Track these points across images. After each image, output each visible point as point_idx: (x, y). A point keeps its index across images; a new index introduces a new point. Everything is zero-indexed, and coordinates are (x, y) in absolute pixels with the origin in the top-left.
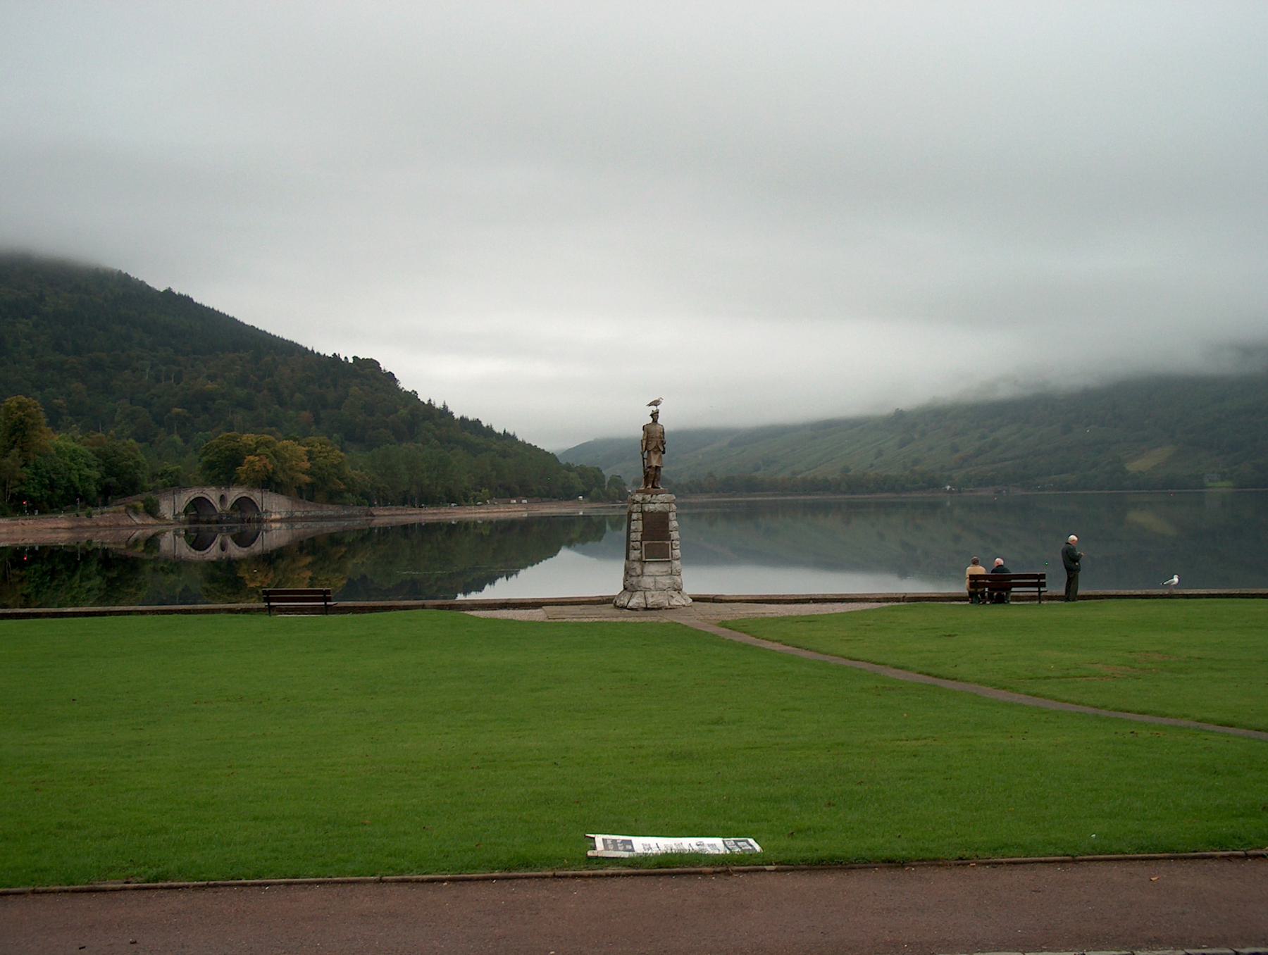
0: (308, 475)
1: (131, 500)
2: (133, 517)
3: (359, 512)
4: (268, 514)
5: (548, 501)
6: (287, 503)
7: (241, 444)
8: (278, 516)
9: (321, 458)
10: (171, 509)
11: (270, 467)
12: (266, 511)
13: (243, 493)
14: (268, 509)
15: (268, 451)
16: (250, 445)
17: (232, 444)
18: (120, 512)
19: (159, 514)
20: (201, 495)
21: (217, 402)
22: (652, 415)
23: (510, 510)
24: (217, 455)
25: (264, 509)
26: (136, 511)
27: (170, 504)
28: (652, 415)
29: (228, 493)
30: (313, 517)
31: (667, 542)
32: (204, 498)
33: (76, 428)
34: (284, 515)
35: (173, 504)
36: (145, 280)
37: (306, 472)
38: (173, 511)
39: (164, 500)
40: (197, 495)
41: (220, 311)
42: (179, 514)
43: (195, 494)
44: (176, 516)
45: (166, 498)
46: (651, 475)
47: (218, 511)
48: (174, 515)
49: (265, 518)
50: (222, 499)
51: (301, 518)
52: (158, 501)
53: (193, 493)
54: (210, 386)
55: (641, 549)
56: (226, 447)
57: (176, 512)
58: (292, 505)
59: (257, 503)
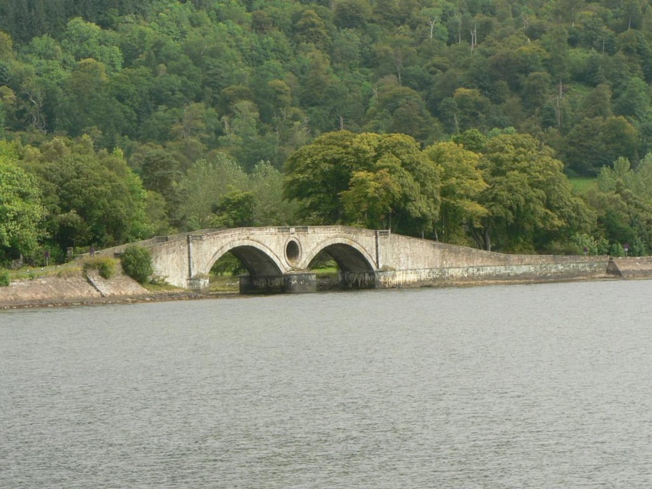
0: (480, 202)
1: (107, 255)
2: (95, 283)
3: (590, 266)
4: (390, 273)
5: (614, 278)
6: (431, 254)
7: (350, 150)
8: (412, 277)
9: (516, 172)
10: (182, 269)
11: (396, 189)
12: (385, 269)
13: (336, 237)
14: (388, 264)
15: (396, 163)
16: (365, 152)
18: (70, 275)
19: (150, 278)
20: (246, 243)
25: (381, 266)
26: (104, 273)
27: (182, 259)
30: (489, 277)
32: (253, 248)
33: (300, 128)
34: (424, 275)
37: (481, 200)
39: (167, 253)
40: (237, 244)
42: (198, 277)
43: (336, 237)
44: (192, 280)
45: (171, 249)
46: (31, 253)
48: (190, 278)
49: (382, 280)
50: (292, 250)
51: (462, 279)
52: (147, 255)
53: (230, 239)
54: (529, 47)
57: (194, 274)
58: (443, 257)
59: (365, 255)
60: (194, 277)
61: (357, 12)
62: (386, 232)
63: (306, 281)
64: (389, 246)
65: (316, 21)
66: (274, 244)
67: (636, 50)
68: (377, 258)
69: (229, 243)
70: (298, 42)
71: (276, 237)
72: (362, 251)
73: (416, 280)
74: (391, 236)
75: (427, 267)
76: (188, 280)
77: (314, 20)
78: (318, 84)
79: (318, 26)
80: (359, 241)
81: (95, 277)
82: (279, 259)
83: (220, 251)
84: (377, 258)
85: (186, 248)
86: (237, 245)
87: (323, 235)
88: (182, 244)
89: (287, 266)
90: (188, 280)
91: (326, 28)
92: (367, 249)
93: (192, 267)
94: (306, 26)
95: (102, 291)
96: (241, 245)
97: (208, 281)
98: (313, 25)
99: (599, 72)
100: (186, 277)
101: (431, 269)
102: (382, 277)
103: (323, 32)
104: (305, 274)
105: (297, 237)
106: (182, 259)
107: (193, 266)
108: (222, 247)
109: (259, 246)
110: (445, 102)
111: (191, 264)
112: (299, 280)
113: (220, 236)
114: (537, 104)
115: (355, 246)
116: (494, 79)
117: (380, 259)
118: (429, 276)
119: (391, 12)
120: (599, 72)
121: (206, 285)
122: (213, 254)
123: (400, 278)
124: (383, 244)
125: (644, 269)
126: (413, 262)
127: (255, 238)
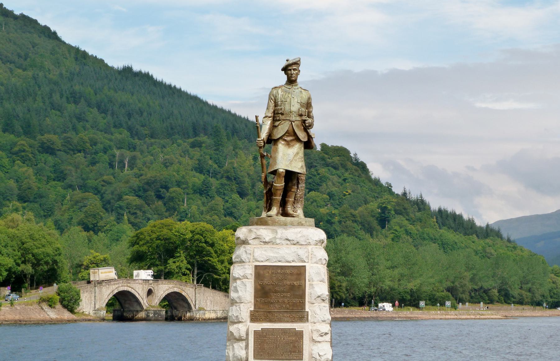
8: (213, 315)
10: (91, 303)
12: (200, 309)
17: (165, 231)
20: (125, 289)
21: (171, 190)
22: (285, 69)
23: (482, 317)
24: (148, 245)
28: (285, 69)
29: (156, 288)
31: (297, 326)
32: (129, 292)
35: (93, 298)
36: (342, 145)
38: (93, 306)
40: (121, 289)
41: (182, 90)
44: (97, 310)
47: (145, 308)
52: (78, 294)
53: (117, 286)
55: (247, 339)
56: (158, 236)
57: (97, 307)
60: (98, 309)
61: (52, 144)
62: (201, 286)
63: (159, 314)
64: (202, 295)
65: (27, 149)
66: (141, 289)
67: (233, 178)
68: (195, 302)
69: (117, 288)
70: (14, 162)
71: (141, 286)
72: (187, 297)
73: (215, 317)
74: (203, 288)
75: (221, 309)
76: (94, 310)
77: (25, 148)
78: (29, 189)
79: (27, 151)
80: (186, 291)
81: (45, 306)
82: (143, 300)
83: (111, 293)
84: (195, 302)
85: (93, 290)
86: (121, 290)
87: (167, 285)
88: (91, 287)
89: (147, 305)
90: (94, 310)
91: (32, 153)
92: (190, 296)
93: (96, 302)
94: (20, 151)
95: (51, 316)
96: (123, 290)
97: (105, 312)
98: (24, 151)
99: (213, 191)
100: (92, 309)
101: (223, 310)
102: (198, 314)
103: (30, 155)
104: (159, 311)
105: (153, 286)
106: (91, 297)
107: (97, 302)
108: (113, 291)
109: (133, 291)
110: (118, 204)
111: (96, 300)
112: (154, 314)
113: (112, 283)
114: (175, 209)
115: (183, 294)
116: (145, 191)
117: (197, 302)
118: (222, 315)
119: (71, 145)
120: (213, 191)
121: (104, 315)
122: (108, 295)
123: (208, 316)
124: (199, 293)
125: (336, 316)
126: (214, 305)
127: (131, 286)
